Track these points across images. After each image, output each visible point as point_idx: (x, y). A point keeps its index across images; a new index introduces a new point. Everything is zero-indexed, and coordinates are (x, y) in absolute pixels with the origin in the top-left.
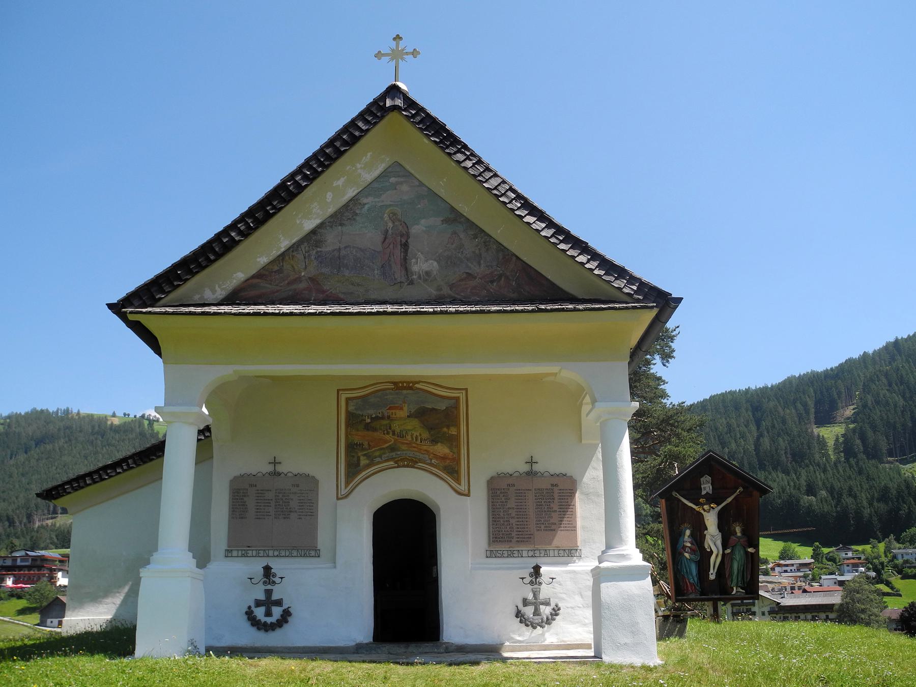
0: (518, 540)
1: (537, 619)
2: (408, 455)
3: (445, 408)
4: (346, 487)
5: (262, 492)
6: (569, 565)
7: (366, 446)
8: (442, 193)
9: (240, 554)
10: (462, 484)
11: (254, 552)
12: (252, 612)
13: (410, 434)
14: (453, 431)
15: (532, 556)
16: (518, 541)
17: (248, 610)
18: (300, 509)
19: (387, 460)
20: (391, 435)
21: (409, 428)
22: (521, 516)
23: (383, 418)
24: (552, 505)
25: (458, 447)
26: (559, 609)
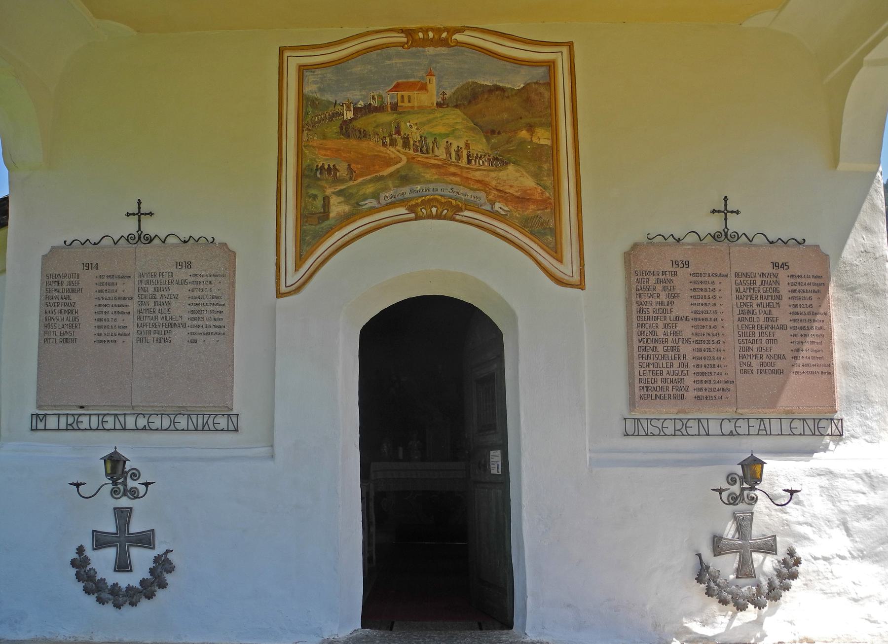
0: (700, 393)
1: (747, 588)
2: (440, 192)
3: (522, 86)
4: (297, 268)
5: (110, 280)
6: (815, 455)
7: (343, 172)
9: (63, 425)
10: (564, 260)
11: (94, 419)
12: (86, 561)
13: (443, 143)
14: (542, 137)
15: (731, 434)
16: (698, 398)
17: (77, 556)
18: (194, 319)
19: (390, 203)
20: (399, 147)
21: (440, 129)
22: (705, 338)
23: (380, 109)
24: (775, 312)
25: (555, 172)
26: (798, 562)
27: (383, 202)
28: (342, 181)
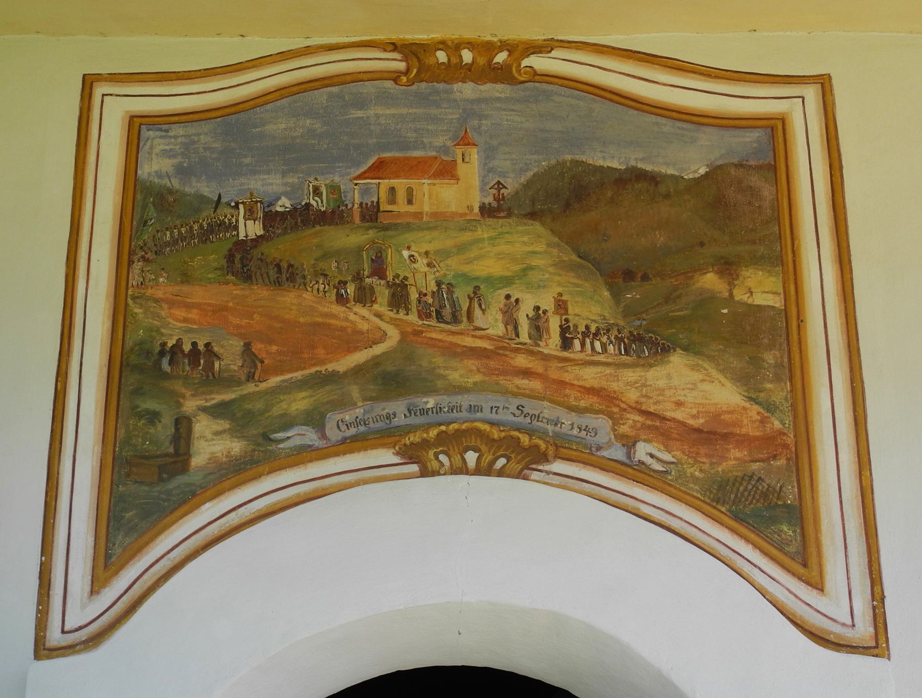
4: (96, 585)
13: (497, 300)
20: (381, 306)
27: (334, 434)
28: (228, 381)
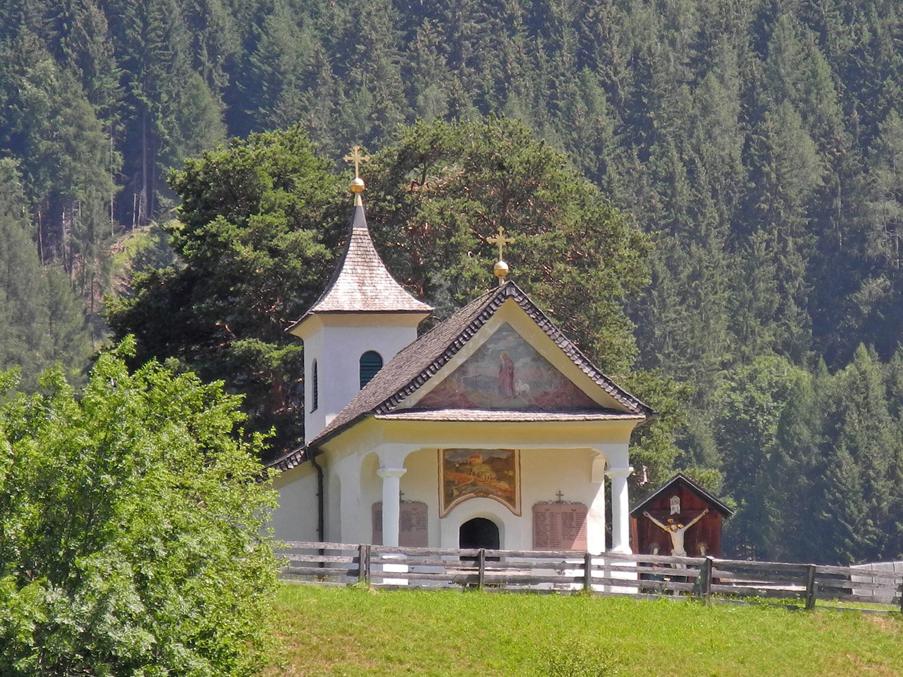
8: (531, 342)
23: (466, 464)
